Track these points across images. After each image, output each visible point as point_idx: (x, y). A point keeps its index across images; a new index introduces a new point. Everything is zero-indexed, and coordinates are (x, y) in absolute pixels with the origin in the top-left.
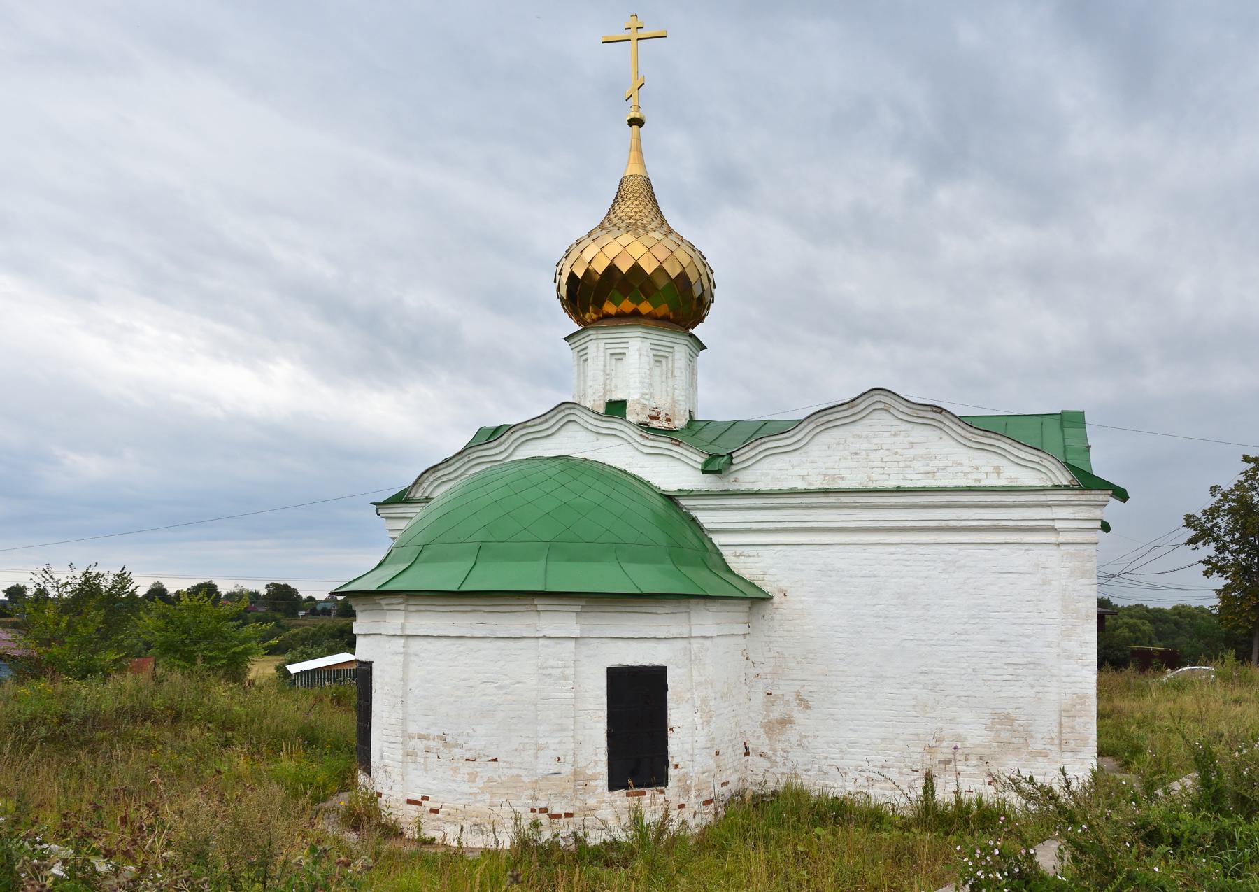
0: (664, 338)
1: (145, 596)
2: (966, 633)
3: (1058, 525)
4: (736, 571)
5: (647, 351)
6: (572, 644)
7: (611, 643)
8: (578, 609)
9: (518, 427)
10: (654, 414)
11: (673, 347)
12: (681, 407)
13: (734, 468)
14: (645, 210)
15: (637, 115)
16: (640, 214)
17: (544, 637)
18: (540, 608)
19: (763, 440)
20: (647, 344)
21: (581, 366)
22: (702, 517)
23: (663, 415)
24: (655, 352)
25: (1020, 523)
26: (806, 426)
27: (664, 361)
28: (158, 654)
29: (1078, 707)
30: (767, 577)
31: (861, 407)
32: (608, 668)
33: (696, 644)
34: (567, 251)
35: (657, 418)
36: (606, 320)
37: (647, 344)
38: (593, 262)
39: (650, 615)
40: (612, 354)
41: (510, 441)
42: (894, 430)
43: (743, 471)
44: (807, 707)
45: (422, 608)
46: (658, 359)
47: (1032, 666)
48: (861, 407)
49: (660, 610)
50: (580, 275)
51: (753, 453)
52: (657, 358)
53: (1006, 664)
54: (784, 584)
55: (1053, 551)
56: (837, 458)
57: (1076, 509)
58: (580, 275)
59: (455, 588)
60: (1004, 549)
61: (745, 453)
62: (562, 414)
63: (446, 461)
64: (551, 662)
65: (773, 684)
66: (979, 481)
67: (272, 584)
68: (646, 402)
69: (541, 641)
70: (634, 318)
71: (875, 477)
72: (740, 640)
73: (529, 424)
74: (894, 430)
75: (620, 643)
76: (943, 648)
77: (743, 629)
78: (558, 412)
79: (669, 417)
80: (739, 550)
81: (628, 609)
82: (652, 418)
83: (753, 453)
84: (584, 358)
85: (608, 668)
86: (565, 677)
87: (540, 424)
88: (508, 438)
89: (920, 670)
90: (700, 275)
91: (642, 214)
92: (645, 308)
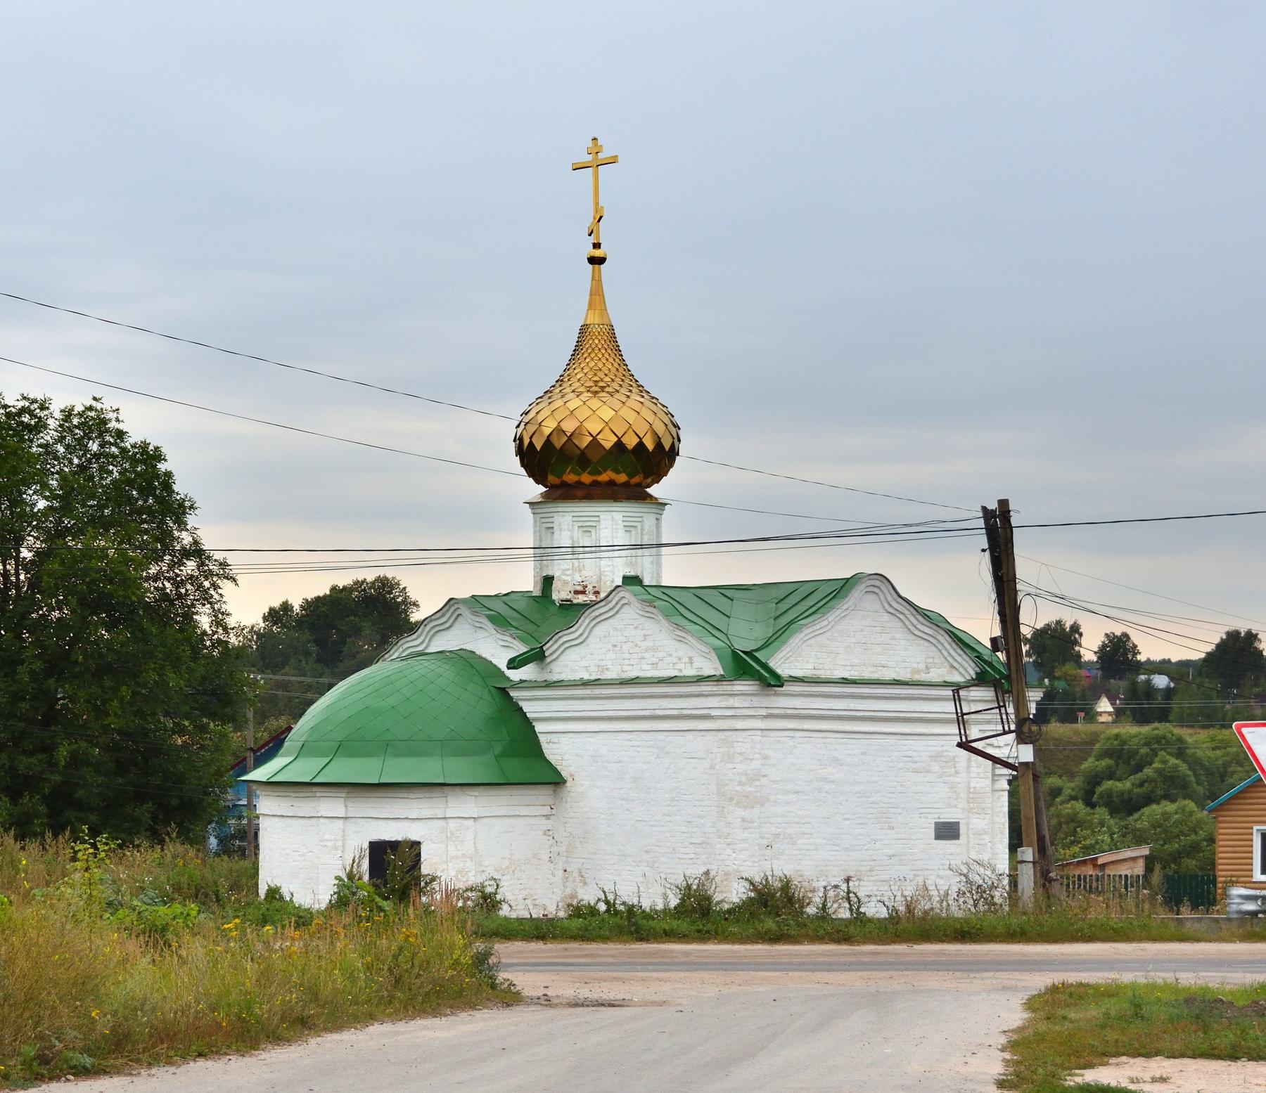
2: (669, 815)
3: (713, 713)
4: (548, 757)
5: (568, 525)
6: (341, 821)
7: (373, 822)
8: (344, 795)
9: (428, 620)
10: (579, 588)
12: (608, 578)
13: (548, 660)
14: (610, 365)
17: (322, 817)
18: (318, 794)
19: (560, 634)
22: (527, 706)
23: (590, 588)
24: (580, 524)
25: (694, 712)
26: (584, 621)
27: (593, 530)
29: (725, 883)
30: (564, 763)
31: (614, 603)
32: (370, 842)
33: (452, 825)
35: (583, 592)
38: (534, 436)
39: (405, 800)
41: (425, 633)
42: (636, 622)
43: (554, 663)
44: (585, 883)
45: (301, 795)
47: (704, 845)
48: (614, 603)
49: (412, 796)
50: (538, 447)
51: (556, 646)
53: (691, 843)
54: (572, 769)
55: (758, 736)
56: (604, 650)
57: (720, 698)
58: (538, 447)
59: (307, 780)
60: (690, 736)
61: (551, 647)
62: (453, 609)
64: (327, 836)
65: (567, 862)
68: (568, 578)
69: (321, 820)
71: (626, 668)
72: (543, 821)
73: (433, 617)
74: (636, 622)
75: (381, 823)
76: (656, 829)
77: (546, 810)
78: (450, 607)
79: (596, 589)
80: (549, 736)
81: (380, 795)
82: (577, 592)
83: (556, 646)
85: (370, 842)
86: (336, 848)
87: (438, 619)
88: (423, 631)
89: (645, 849)
90: (666, 425)
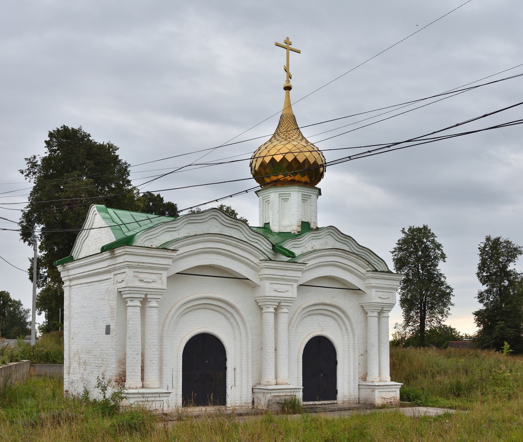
0: (307, 191)
1: (87, 209)
11: (310, 196)
15: (288, 85)
16: (291, 134)
20: (300, 194)
21: (264, 204)
28: (32, 346)
34: (259, 148)
36: (276, 184)
37: (300, 194)
40: (282, 199)
46: (304, 200)
52: (303, 201)
63: (164, 244)
66: (189, 233)
67: (51, 135)
70: (293, 183)
84: (268, 202)
91: (292, 135)
92: (297, 177)
